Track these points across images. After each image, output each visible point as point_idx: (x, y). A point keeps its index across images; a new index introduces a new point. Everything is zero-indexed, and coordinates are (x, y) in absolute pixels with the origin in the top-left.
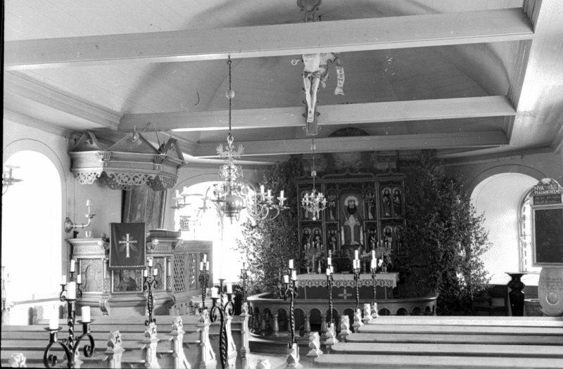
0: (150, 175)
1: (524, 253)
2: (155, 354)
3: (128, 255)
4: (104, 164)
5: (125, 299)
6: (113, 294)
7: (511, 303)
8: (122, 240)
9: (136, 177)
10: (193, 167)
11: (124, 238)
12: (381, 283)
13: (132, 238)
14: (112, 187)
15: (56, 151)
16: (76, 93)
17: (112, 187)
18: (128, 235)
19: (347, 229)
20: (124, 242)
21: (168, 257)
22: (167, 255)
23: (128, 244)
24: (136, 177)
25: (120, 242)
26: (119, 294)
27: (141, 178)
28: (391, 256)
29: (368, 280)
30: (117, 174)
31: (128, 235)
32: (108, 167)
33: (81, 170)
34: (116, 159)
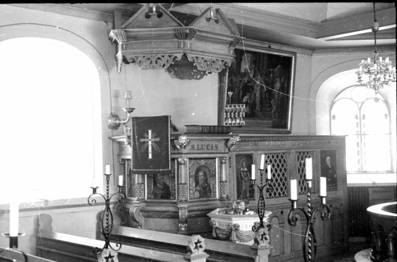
0: (175, 55)
1: (364, 161)
3: (150, 156)
5: (157, 209)
6: (145, 202)
7: (176, 17)
9: (159, 59)
11: (146, 136)
13: (155, 134)
15: (94, 45)
16: (337, 56)
18: (150, 132)
20: (145, 140)
21: (221, 159)
22: (219, 155)
23: (150, 143)
24: (159, 59)
25: (142, 140)
26: (158, 202)
28: (115, 203)
30: (137, 58)
31: (150, 132)
32: (126, 49)
34: (135, 38)
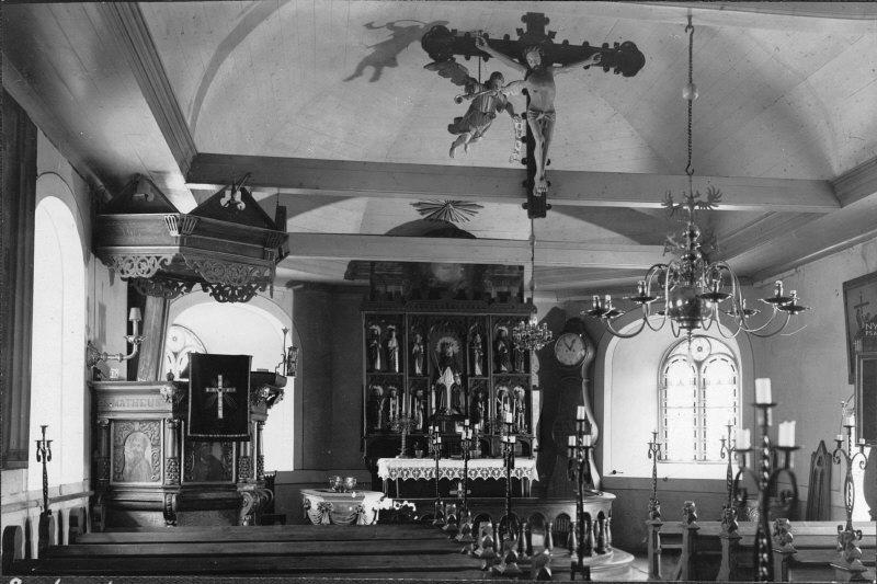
2: (266, 528)
4: (182, 240)
8: (211, 386)
10: (16, 173)
12: (402, 473)
13: (228, 382)
14: (221, 298)
17: (221, 298)
19: (441, 389)
20: (213, 390)
23: (220, 395)
27: (150, 262)
29: (497, 469)
31: (220, 377)
33: (122, 250)
